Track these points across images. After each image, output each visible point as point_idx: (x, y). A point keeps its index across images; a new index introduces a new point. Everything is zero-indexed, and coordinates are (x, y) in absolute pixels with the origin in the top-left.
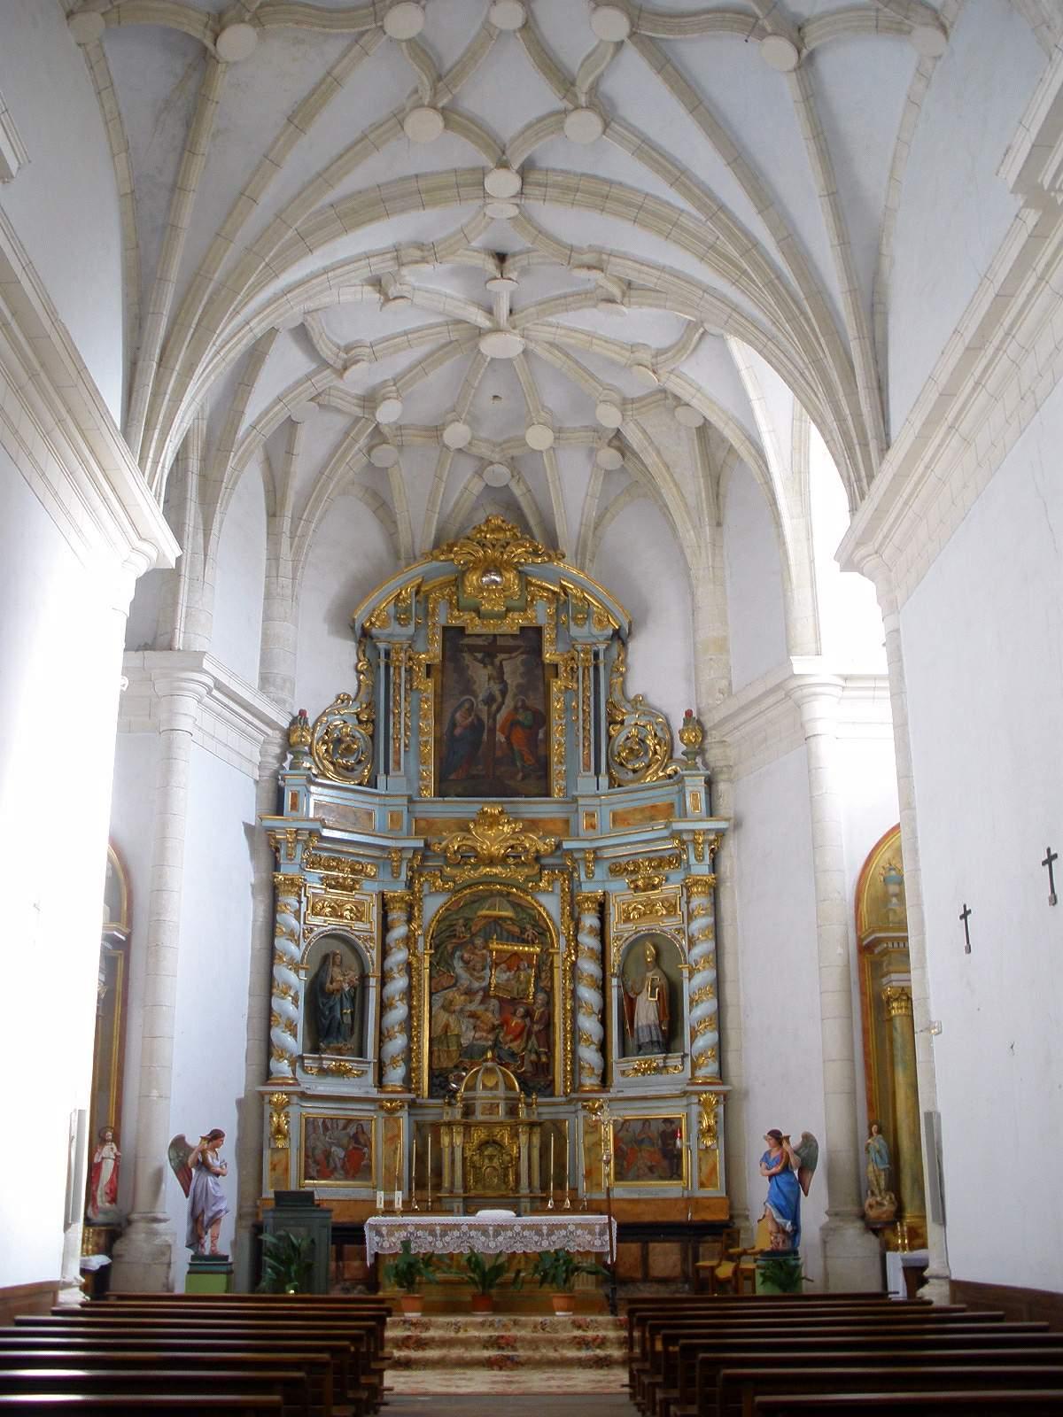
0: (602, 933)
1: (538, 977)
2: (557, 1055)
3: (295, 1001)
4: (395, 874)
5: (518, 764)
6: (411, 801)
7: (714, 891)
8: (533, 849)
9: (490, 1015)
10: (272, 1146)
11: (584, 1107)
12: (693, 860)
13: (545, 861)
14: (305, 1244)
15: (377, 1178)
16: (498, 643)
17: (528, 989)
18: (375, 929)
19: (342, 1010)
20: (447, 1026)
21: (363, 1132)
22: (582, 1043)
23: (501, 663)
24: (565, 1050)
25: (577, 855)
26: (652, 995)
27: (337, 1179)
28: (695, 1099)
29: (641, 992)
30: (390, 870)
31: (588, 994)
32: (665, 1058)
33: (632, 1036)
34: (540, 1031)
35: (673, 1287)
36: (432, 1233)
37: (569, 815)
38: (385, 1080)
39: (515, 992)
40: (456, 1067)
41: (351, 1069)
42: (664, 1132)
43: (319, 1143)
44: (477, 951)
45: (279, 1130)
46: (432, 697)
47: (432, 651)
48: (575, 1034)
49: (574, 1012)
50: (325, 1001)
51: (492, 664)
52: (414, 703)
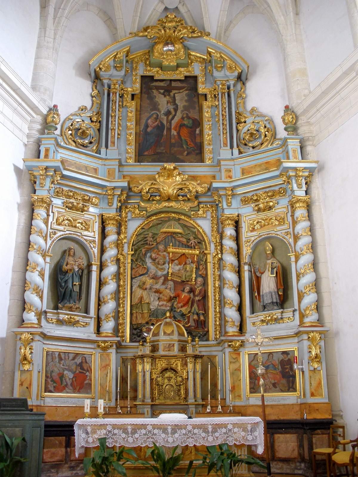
0: (237, 239)
1: (197, 269)
2: (210, 315)
3: (42, 275)
4: (110, 204)
5: (185, 147)
6: (120, 165)
7: (309, 207)
8: (194, 190)
9: (168, 291)
10: (21, 369)
11: (229, 346)
12: (295, 186)
13: (202, 199)
14: (16, 442)
15: (95, 393)
16: (173, 85)
17: (191, 275)
18: (97, 236)
19: (73, 282)
20: (142, 298)
21: (86, 362)
22: (227, 306)
23: (174, 94)
24: (215, 312)
25: (222, 192)
26: (272, 273)
27: (68, 393)
28: (305, 337)
29: (264, 272)
30: (107, 201)
31: (230, 276)
32: (282, 313)
33: (260, 301)
34: (199, 300)
35: (293, 466)
36: (125, 431)
37: (215, 173)
38: (101, 329)
39: (184, 277)
40: (147, 323)
41: (78, 321)
42: (282, 360)
43: (56, 369)
44: (160, 253)
45: (25, 358)
46: (134, 110)
47: (136, 87)
48: (222, 302)
49: (221, 288)
50: (63, 277)
51: (169, 95)
52: (124, 114)
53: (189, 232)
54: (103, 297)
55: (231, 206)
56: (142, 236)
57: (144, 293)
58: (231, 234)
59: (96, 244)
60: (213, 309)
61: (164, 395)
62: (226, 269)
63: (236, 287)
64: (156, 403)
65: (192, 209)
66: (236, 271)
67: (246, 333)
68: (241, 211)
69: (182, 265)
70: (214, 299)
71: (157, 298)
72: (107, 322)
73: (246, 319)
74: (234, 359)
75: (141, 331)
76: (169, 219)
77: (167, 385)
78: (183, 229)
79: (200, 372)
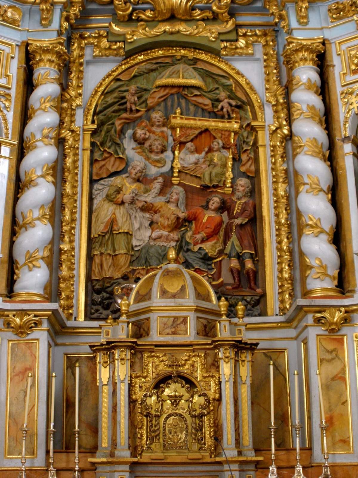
1: (236, 160)
9: (172, 207)
11: (318, 321)
17: (224, 174)
20: (113, 222)
22: (307, 231)
30: (37, 17)
34: (241, 226)
38: (17, 287)
40: (125, 278)
44: (154, 129)
53: (217, 86)
54: (22, 213)
55: (307, 23)
56: (116, 94)
57: (117, 212)
58: (309, 80)
59: (10, 101)
60: (275, 245)
61: (161, 440)
62: (303, 153)
63: (325, 189)
64: (142, 460)
65: (223, 37)
66: (324, 155)
67: (353, 291)
68: (328, 35)
69: (204, 153)
70: (276, 222)
71: (147, 224)
72: (30, 270)
73: (353, 262)
74: (331, 352)
75: (112, 295)
76: (175, 61)
77: (170, 415)
78: (205, 81)
79: (249, 382)
